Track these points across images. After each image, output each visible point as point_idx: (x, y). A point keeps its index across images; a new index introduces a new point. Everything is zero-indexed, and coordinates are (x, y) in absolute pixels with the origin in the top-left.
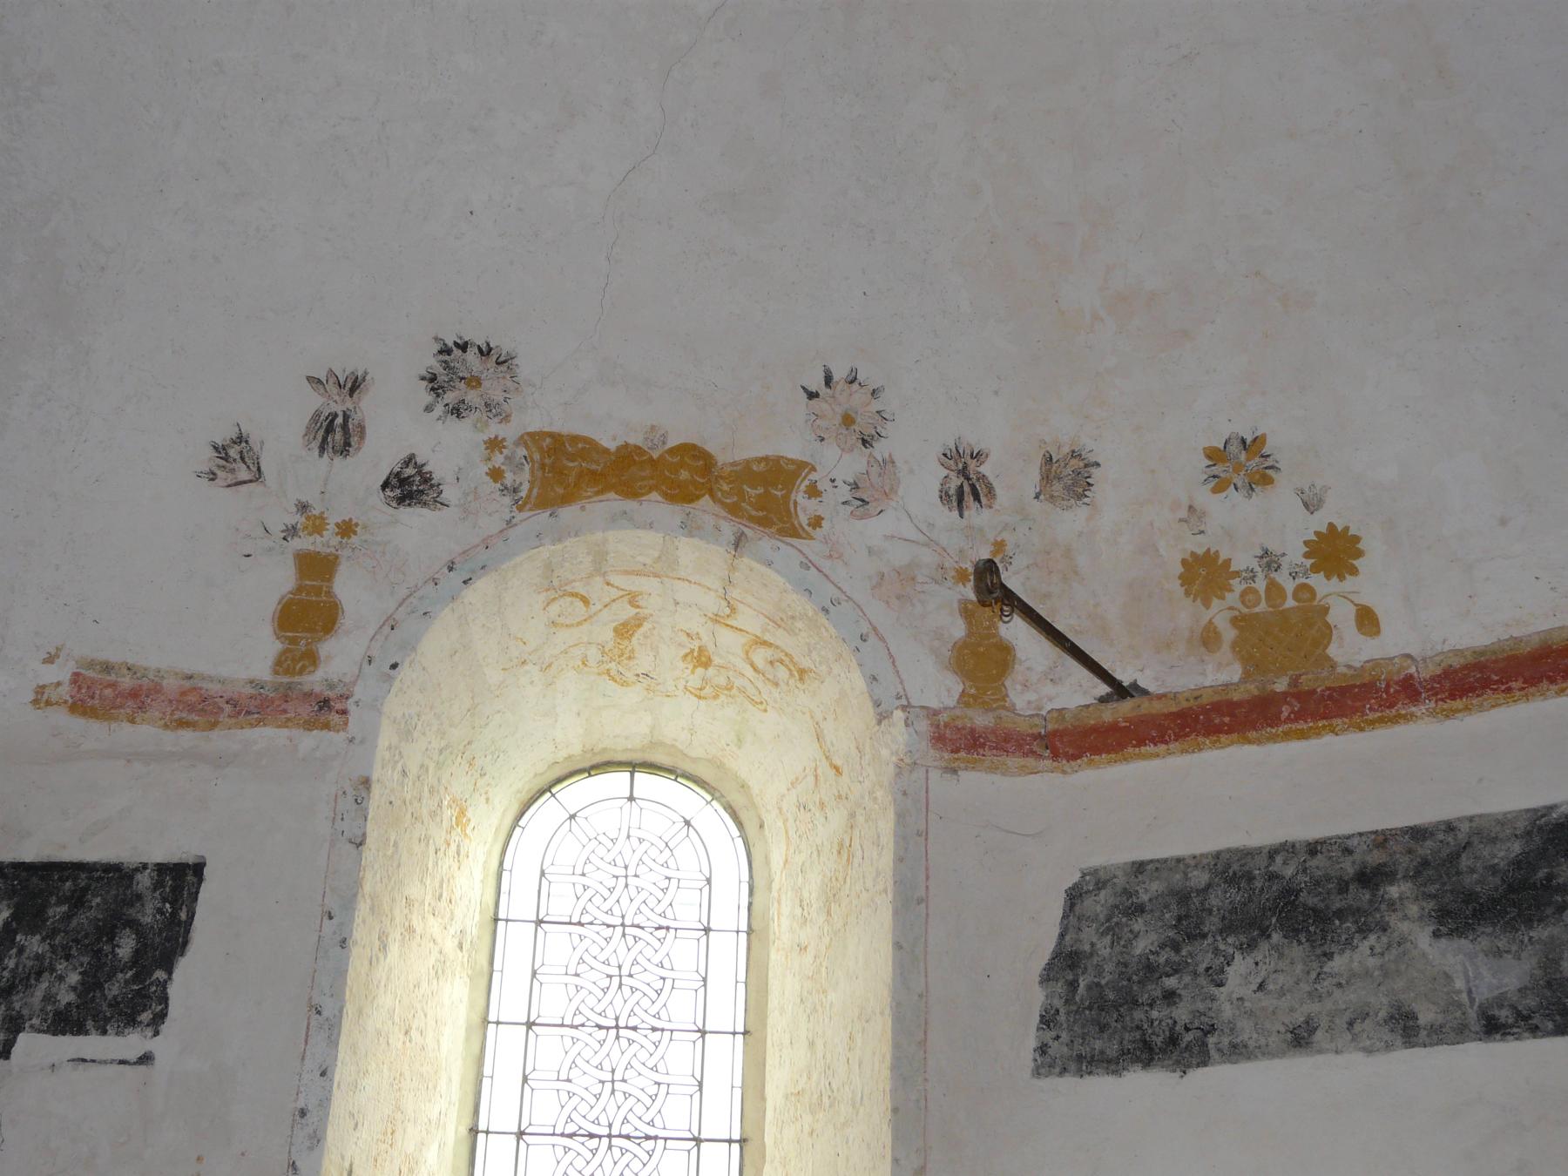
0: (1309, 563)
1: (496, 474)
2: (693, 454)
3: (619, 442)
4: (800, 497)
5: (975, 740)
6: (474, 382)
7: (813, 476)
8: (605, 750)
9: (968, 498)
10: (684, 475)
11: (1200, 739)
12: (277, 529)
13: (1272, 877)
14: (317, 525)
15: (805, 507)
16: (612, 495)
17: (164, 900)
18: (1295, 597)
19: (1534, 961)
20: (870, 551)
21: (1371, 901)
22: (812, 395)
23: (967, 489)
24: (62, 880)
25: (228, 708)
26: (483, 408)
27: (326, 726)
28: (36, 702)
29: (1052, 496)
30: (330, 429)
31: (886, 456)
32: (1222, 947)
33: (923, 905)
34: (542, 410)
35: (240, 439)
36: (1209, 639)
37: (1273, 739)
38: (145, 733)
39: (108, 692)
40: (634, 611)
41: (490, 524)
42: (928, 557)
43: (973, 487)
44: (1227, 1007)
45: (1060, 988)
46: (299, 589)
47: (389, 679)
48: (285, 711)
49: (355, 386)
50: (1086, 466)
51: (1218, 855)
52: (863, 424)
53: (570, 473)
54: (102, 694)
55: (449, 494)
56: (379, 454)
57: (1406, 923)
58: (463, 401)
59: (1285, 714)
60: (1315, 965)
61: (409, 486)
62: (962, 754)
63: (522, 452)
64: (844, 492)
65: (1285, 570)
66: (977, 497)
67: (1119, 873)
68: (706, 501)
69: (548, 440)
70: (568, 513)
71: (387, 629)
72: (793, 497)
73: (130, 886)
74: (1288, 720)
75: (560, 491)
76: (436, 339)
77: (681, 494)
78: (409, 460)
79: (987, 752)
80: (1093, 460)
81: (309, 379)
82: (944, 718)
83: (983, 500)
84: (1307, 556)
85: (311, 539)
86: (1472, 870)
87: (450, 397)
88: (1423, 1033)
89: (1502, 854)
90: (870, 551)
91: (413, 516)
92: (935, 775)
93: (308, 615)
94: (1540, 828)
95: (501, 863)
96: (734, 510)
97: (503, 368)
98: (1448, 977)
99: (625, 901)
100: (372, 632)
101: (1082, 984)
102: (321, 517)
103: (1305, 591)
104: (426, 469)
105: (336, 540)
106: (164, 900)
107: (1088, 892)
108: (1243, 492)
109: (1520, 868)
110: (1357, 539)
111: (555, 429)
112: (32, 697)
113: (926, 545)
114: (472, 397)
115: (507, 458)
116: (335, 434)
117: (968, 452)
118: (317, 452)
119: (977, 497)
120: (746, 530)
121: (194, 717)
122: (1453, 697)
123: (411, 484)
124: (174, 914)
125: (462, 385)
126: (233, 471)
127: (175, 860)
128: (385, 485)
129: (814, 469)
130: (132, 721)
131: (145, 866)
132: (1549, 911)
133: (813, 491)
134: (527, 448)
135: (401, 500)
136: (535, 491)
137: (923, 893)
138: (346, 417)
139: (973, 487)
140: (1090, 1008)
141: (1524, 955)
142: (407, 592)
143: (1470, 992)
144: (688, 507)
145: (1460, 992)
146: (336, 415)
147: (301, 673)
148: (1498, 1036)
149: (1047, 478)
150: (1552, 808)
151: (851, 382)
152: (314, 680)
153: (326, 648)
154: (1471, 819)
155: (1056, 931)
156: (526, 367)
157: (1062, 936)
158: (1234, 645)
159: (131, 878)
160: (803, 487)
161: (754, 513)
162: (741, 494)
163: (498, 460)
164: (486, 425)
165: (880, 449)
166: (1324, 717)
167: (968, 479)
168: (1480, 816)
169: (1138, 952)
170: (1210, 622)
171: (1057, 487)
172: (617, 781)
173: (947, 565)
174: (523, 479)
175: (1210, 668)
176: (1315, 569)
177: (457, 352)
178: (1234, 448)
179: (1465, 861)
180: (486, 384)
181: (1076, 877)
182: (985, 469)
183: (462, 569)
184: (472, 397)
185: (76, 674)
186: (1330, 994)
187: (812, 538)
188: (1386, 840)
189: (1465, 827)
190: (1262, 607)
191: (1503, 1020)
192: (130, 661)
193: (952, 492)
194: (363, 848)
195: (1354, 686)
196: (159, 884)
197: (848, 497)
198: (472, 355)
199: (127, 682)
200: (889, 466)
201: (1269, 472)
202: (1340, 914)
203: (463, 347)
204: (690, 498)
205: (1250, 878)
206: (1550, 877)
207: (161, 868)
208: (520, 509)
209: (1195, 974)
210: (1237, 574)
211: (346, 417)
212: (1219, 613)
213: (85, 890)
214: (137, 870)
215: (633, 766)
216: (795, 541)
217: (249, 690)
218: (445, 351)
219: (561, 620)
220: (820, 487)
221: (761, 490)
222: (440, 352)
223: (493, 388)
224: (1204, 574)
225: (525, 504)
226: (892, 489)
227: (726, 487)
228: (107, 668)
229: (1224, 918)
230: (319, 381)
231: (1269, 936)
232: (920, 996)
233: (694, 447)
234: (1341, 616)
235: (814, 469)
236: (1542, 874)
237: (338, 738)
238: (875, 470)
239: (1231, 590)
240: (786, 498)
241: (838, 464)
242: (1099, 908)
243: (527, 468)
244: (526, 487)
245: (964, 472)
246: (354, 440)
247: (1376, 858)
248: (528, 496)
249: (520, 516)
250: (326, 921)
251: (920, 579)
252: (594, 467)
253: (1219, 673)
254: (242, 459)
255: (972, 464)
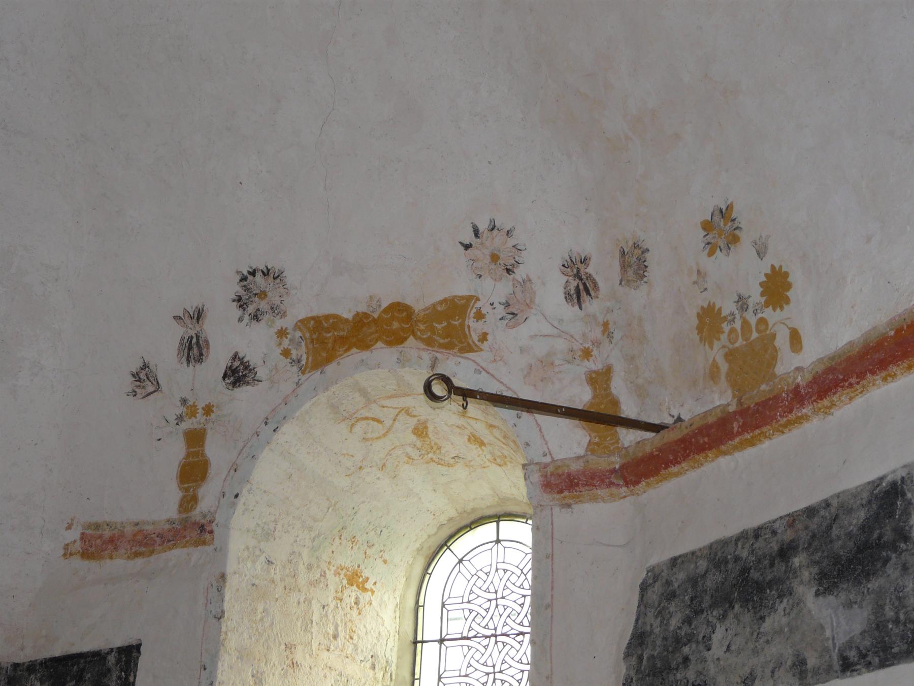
0: (763, 299)
1: (286, 353)
2: (399, 309)
3: (353, 313)
4: (471, 322)
5: (571, 481)
6: (263, 295)
7: (479, 304)
8: (474, 510)
9: (583, 294)
10: (396, 325)
11: (697, 457)
12: (172, 419)
13: (737, 559)
14: (193, 412)
15: (475, 328)
16: (354, 350)
17: (122, 670)
18: (758, 331)
19: (870, 608)
20: (522, 350)
21: (786, 572)
22: (467, 247)
23: (581, 287)
24: (73, 665)
25: (158, 540)
26: (270, 311)
27: (204, 543)
28: (65, 555)
29: (628, 281)
30: (190, 348)
31: (524, 277)
32: (711, 619)
33: (549, 610)
34: (303, 304)
35: (145, 366)
36: (713, 374)
37: (736, 448)
38: (118, 565)
39: (98, 541)
40: (416, 419)
41: (287, 388)
42: (561, 345)
43: (585, 285)
44: (712, 666)
45: (634, 661)
46: (188, 455)
47: (233, 505)
48: (185, 537)
49: (199, 315)
50: (643, 253)
51: (710, 547)
52: (506, 258)
53: (331, 340)
54: (98, 543)
55: (261, 373)
56: (218, 360)
57: (802, 586)
58: (258, 310)
59: (736, 429)
60: (756, 627)
61: (238, 374)
62: (566, 493)
63: (298, 334)
64: (500, 310)
65: (751, 310)
66: (588, 293)
67: (664, 568)
68: (411, 340)
69: (312, 322)
70: (330, 368)
71: (232, 471)
72: (466, 323)
73: (104, 664)
74: (739, 434)
75: (324, 354)
76: (238, 272)
77: (395, 339)
78: (235, 357)
79: (581, 489)
80: (645, 247)
81: (174, 317)
82: (550, 469)
83: (592, 293)
84: (762, 294)
85: (191, 421)
86: (839, 538)
87: (251, 309)
88: (810, 675)
89: (855, 521)
90: (522, 350)
91: (244, 392)
92: (556, 510)
93: (193, 472)
94: (876, 497)
95: (417, 602)
96: (429, 342)
97: (278, 281)
98: (822, 627)
99: (496, 619)
100: (224, 476)
101: (645, 657)
102: (194, 406)
103: (762, 321)
104: (245, 360)
105: (203, 419)
106: (122, 670)
107: (650, 585)
108: (724, 251)
109: (864, 532)
110: (786, 274)
111: (314, 314)
112: (62, 552)
113: (560, 336)
114: (264, 305)
115: (290, 340)
116: (194, 350)
117: (578, 259)
118: (186, 364)
119: (588, 293)
120: (438, 355)
121: (143, 549)
122: (821, 397)
123: (238, 372)
124: (127, 678)
125: (257, 299)
126: (144, 387)
127: (127, 644)
128: (225, 376)
129: (478, 299)
130: (111, 558)
131: (112, 650)
132: (879, 565)
133: (480, 316)
134: (301, 331)
135: (234, 384)
136: (310, 359)
137: (548, 600)
138: (198, 337)
139: (585, 285)
140: (648, 675)
141: (864, 603)
142: (242, 444)
143: (833, 638)
144: (400, 347)
145: (828, 639)
146: (192, 337)
147: (191, 511)
148: (849, 674)
149: (624, 267)
150: (882, 479)
151: (492, 230)
152: (196, 514)
153: (201, 492)
154: (838, 496)
155: (634, 618)
156: (291, 278)
157: (637, 620)
158: (728, 375)
159: (105, 658)
160: (472, 315)
161: (442, 341)
162: (432, 330)
163: (286, 343)
164: (273, 322)
165: (520, 273)
166: (758, 427)
167: (581, 279)
168: (844, 492)
169: (672, 628)
170: (714, 360)
171: (630, 272)
172: (487, 531)
173: (575, 348)
174: (301, 352)
175: (716, 396)
176: (767, 304)
177: (250, 278)
178: (717, 218)
179: (835, 531)
180: (270, 294)
181: (644, 575)
182: (590, 270)
183: (272, 422)
184: (264, 305)
185: (83, 534)
186: (763, 649)
187: (481, 350)
188: (794, 521)
189: (835, 503)
190: (740, 342)
191: (851, 660)
192: (107, 520)
193: (573, 292)
194: (222, 620)
195: (770, 399)
196: (118, 661)
197: (504, 314)
198: (259, 277)
199: (107, 533)
200: (528, 284)
201: (737, 232)
202: (770, 584)
203: (253, 273)
204: (400, 340)
205: (727, 562)
206: (879, 538)
207: (121, 650)
208: (303, 373)
209: (698, 642)
210: (725, 318)
211: (198, 337)
212: (716, 353)
213: (84, 669)
214: (108, 653)
215: (498, 518)
216: (471, 355)
217: (167, 526)
218: (244, 279)
219: (369, 436)
220: (484, 311)
221: (445, 324)
222: (241, 281)
223: (274, 297)
224: (709, 321)
225: (305, 370)
226: (531, 301)
227: (422, 327)
228: (97, 526)
229: (712, 596)
230: (180, 318)
231: (733, 607)
232: (547, 678)
233: (398, 304)
234: (782, 340)
235: (478, 299)
236: (875, 535)
237: (209, 549)
238: (518, 290)
239: (723, 332)
240: (462, 325)
241: (493, 291)
242: (655, 597)
243: (303, 344)
244: (304, 357)
245: (578, 276)
246: (204, 351)
247: (789, 536)
248: (307, 363)
249: (303, 378)
250: (203, 671)
251: (557, 362)
252: (342, 333)
253: (720, 398)
254: (148, 378)
255: (582, 267)
